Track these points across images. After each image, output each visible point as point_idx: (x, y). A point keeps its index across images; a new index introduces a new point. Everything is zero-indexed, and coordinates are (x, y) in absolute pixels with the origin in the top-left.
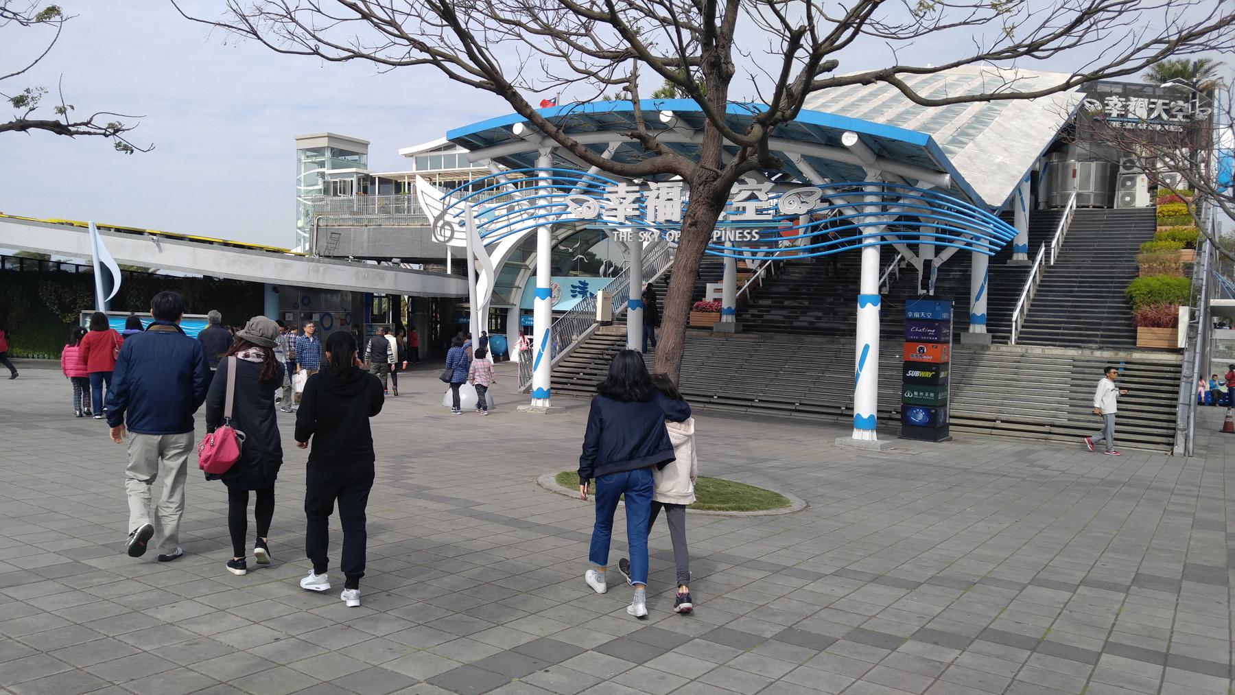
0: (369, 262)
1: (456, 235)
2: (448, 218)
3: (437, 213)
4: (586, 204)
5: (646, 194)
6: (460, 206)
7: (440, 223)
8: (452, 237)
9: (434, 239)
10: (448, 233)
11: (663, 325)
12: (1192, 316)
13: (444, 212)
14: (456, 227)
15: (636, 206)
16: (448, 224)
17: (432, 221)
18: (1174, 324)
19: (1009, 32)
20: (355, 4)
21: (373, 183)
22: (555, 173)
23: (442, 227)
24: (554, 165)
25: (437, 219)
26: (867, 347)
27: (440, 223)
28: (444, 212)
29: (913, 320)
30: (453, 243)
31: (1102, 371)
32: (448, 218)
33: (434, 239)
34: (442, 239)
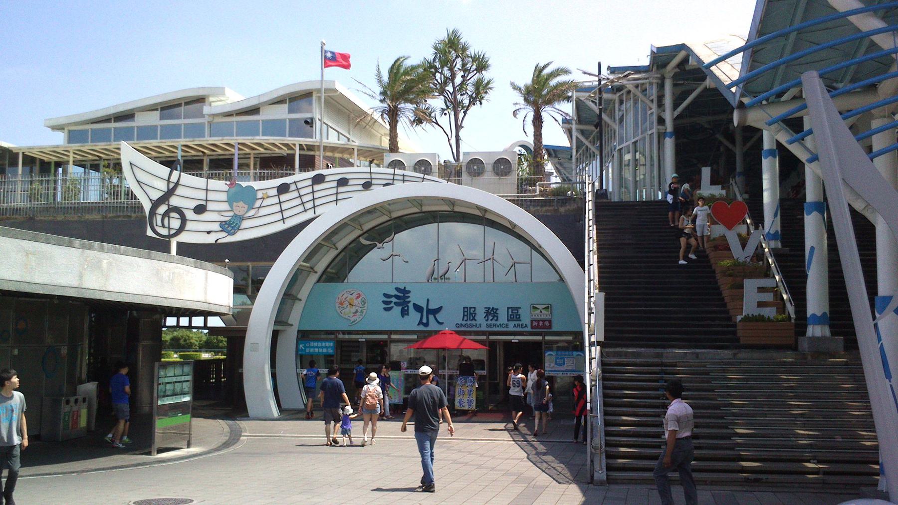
1: (189, 226)
2: (174, 201)
3: (156, 195)
6: (192, 187)
7: (162, 209)
10: (176, 224)
11: (649, 53)
12: (55, 196)
13: (170, 193)
14: (189, 215)
16: (177, 210)
17: (147, 206)
18: (721, 143)
20: (872, 228)
21: (14, 163)
23: (166, 214)
25: (156, 204)
26: (812, 249)
27: (162, 209)
28: (170, 193)
29: (738, 444)
32: (174, 201)
34: (164, 232)
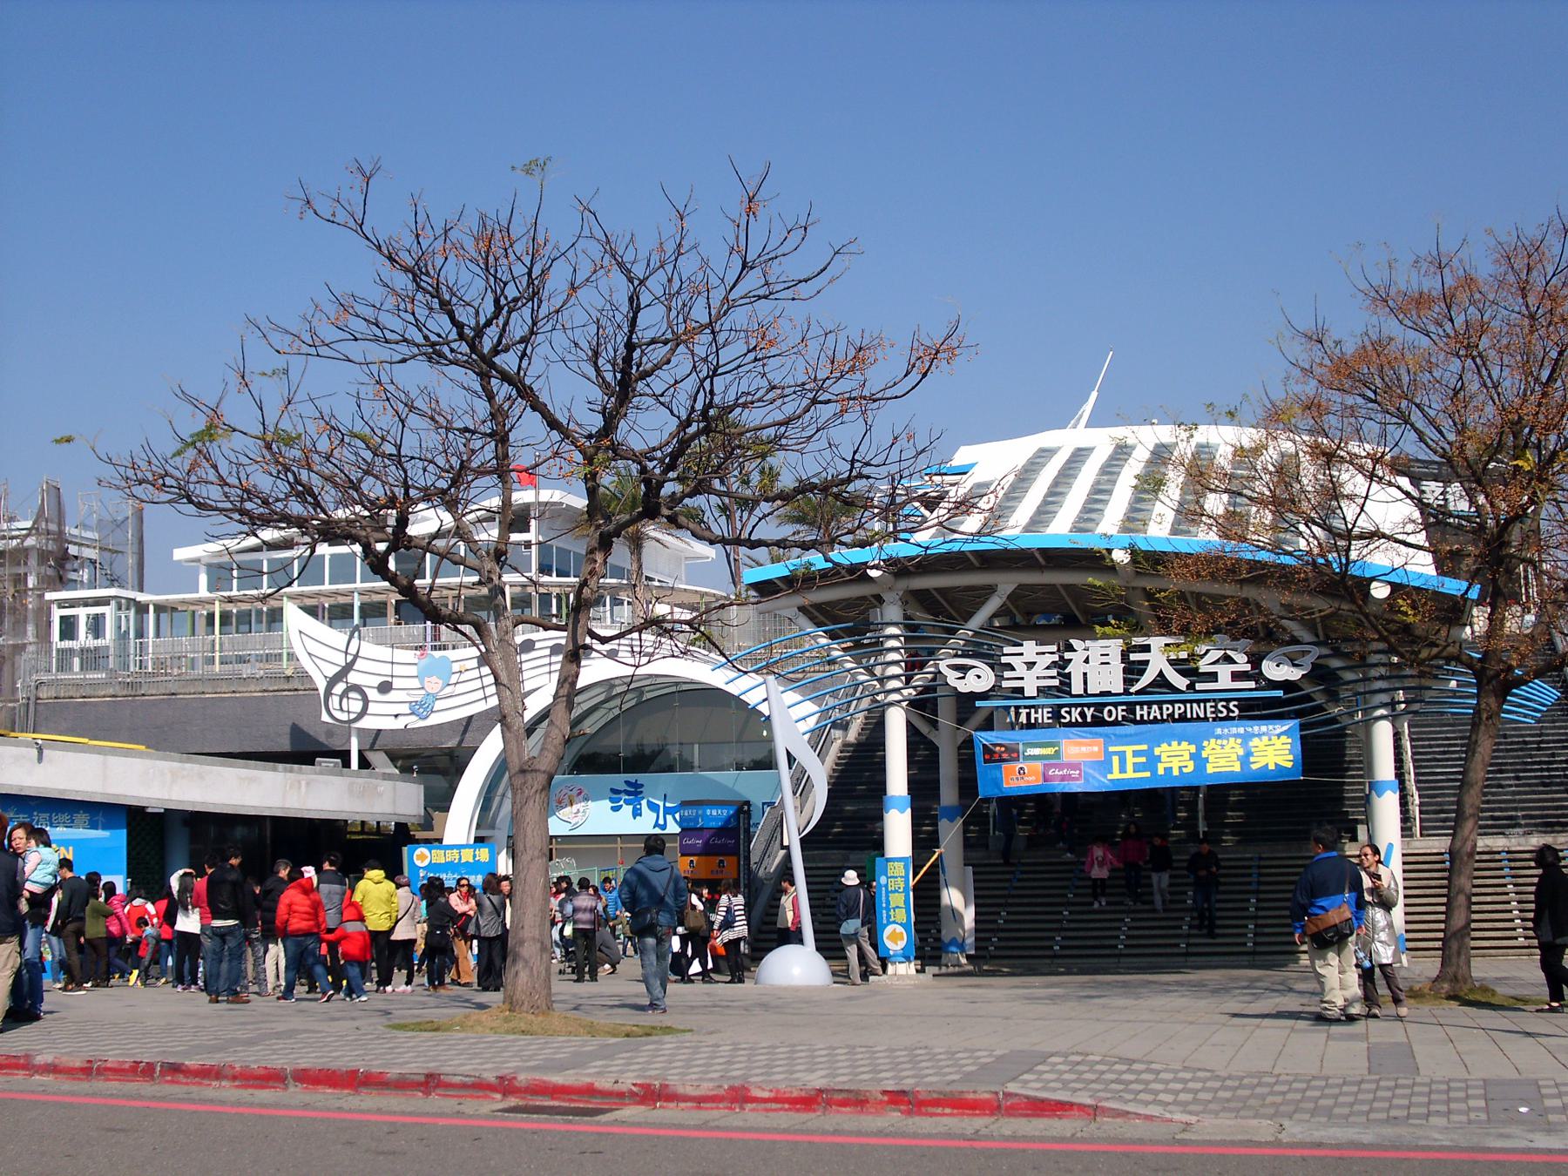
0: (766, 1095)
1: (372, 708)
3: (331, 671)
4: (971, 673)
5: (1067, 655)
7: (339, 688)
8: (363, 713)
9: (325, 718)
10: (356, 706)
14: (372, 694)
15: (1054, 672)
16: (357, 688)
17: (321, 685)
19: (881, 547)
22: (908, 627)
24: (906, 617)
30: (367, 723)
31: (397, 683)
33: (325, 718)
34: (343, 717)
